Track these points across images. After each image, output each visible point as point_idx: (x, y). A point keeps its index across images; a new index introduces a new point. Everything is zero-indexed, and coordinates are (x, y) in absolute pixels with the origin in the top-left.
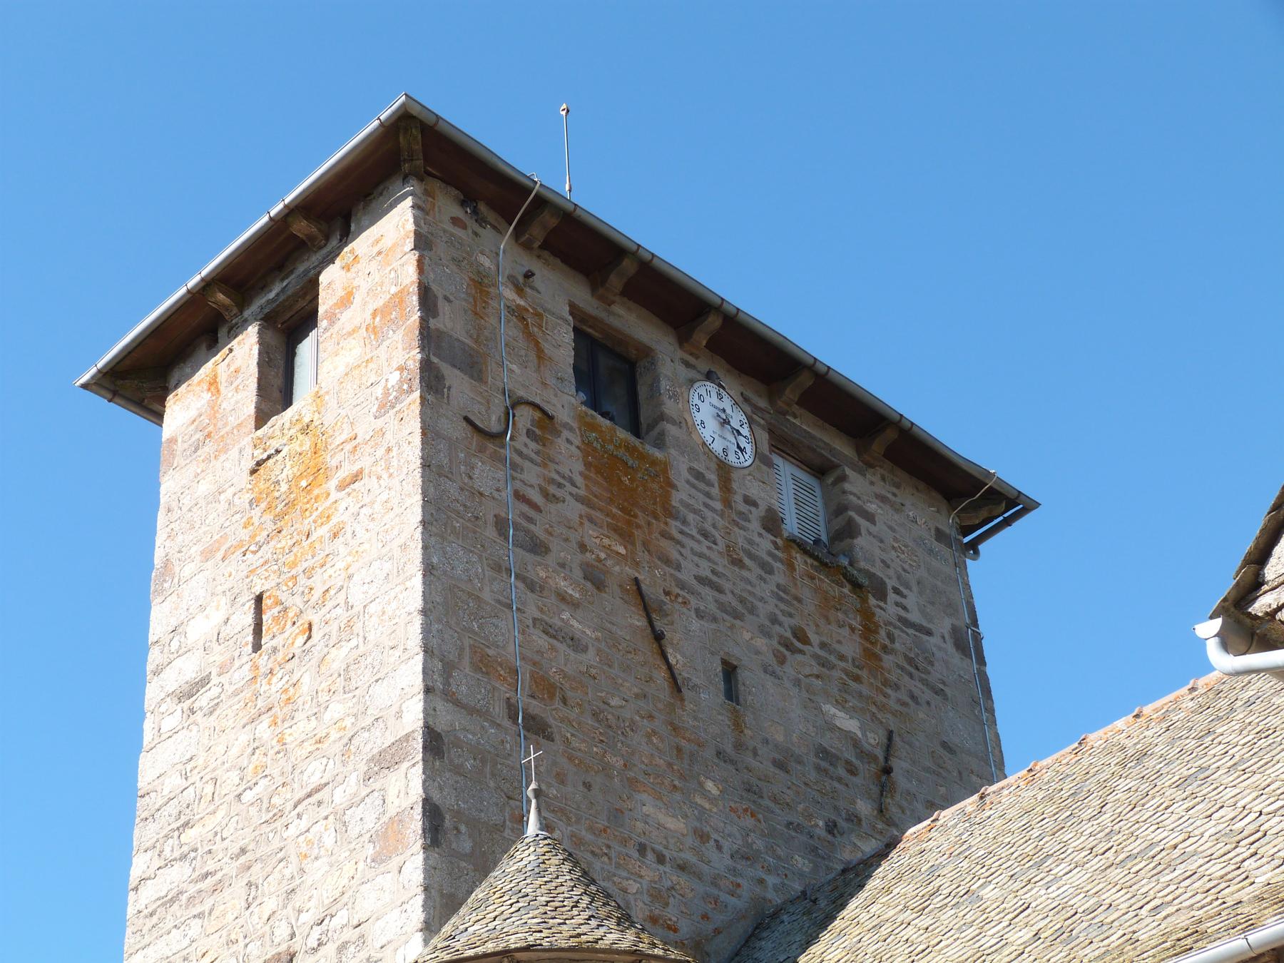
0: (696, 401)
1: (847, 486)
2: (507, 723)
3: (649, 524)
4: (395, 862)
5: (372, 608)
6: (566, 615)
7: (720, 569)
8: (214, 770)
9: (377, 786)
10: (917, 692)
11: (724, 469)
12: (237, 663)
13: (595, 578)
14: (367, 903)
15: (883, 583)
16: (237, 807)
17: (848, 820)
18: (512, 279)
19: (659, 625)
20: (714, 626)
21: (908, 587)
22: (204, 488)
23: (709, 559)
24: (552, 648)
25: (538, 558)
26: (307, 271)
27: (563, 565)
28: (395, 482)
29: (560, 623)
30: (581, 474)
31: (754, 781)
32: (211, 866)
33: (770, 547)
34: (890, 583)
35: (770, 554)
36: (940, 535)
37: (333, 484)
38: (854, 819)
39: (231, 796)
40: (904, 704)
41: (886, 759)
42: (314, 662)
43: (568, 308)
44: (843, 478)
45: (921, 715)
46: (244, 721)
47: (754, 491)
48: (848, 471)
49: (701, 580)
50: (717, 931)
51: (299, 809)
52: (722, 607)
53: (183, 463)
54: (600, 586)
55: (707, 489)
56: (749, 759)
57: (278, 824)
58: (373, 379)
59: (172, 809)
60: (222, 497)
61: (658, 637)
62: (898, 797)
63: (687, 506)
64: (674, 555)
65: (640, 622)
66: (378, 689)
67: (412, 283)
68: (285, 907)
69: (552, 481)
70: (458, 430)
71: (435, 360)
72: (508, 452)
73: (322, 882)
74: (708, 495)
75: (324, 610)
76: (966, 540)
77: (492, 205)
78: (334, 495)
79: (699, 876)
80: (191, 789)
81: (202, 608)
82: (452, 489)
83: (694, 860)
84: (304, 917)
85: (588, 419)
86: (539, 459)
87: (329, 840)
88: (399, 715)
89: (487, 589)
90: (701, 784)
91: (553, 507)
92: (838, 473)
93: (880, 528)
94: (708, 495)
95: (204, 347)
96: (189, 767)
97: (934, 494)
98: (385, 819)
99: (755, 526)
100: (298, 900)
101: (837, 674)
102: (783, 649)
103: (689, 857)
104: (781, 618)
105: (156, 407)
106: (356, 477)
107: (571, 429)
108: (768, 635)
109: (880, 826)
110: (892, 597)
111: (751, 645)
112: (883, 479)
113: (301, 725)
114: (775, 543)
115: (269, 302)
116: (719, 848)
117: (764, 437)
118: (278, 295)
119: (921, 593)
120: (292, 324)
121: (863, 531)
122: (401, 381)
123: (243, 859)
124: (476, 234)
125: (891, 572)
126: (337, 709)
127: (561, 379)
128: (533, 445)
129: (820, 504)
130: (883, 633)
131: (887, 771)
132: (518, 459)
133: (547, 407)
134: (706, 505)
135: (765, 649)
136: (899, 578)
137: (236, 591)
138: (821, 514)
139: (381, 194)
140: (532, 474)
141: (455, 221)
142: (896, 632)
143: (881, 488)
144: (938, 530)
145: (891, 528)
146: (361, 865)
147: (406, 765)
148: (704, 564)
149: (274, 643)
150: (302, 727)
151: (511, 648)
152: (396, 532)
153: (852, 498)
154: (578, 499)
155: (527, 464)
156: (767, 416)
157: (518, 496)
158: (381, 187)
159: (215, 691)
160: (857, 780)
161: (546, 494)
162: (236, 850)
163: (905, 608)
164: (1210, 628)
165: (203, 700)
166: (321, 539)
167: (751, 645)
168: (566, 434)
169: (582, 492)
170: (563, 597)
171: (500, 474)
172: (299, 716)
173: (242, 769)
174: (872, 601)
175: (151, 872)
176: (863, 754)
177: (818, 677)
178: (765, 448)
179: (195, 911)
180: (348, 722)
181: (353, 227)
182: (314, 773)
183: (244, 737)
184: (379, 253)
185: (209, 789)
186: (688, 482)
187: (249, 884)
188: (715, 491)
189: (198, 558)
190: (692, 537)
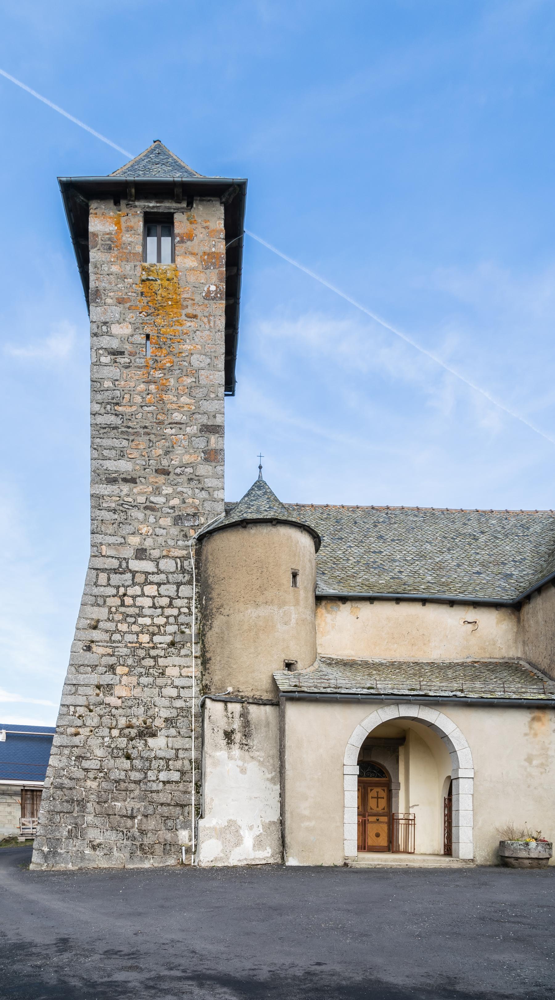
46: (144, 380)
118: (154, 207)
139: (209, 201)
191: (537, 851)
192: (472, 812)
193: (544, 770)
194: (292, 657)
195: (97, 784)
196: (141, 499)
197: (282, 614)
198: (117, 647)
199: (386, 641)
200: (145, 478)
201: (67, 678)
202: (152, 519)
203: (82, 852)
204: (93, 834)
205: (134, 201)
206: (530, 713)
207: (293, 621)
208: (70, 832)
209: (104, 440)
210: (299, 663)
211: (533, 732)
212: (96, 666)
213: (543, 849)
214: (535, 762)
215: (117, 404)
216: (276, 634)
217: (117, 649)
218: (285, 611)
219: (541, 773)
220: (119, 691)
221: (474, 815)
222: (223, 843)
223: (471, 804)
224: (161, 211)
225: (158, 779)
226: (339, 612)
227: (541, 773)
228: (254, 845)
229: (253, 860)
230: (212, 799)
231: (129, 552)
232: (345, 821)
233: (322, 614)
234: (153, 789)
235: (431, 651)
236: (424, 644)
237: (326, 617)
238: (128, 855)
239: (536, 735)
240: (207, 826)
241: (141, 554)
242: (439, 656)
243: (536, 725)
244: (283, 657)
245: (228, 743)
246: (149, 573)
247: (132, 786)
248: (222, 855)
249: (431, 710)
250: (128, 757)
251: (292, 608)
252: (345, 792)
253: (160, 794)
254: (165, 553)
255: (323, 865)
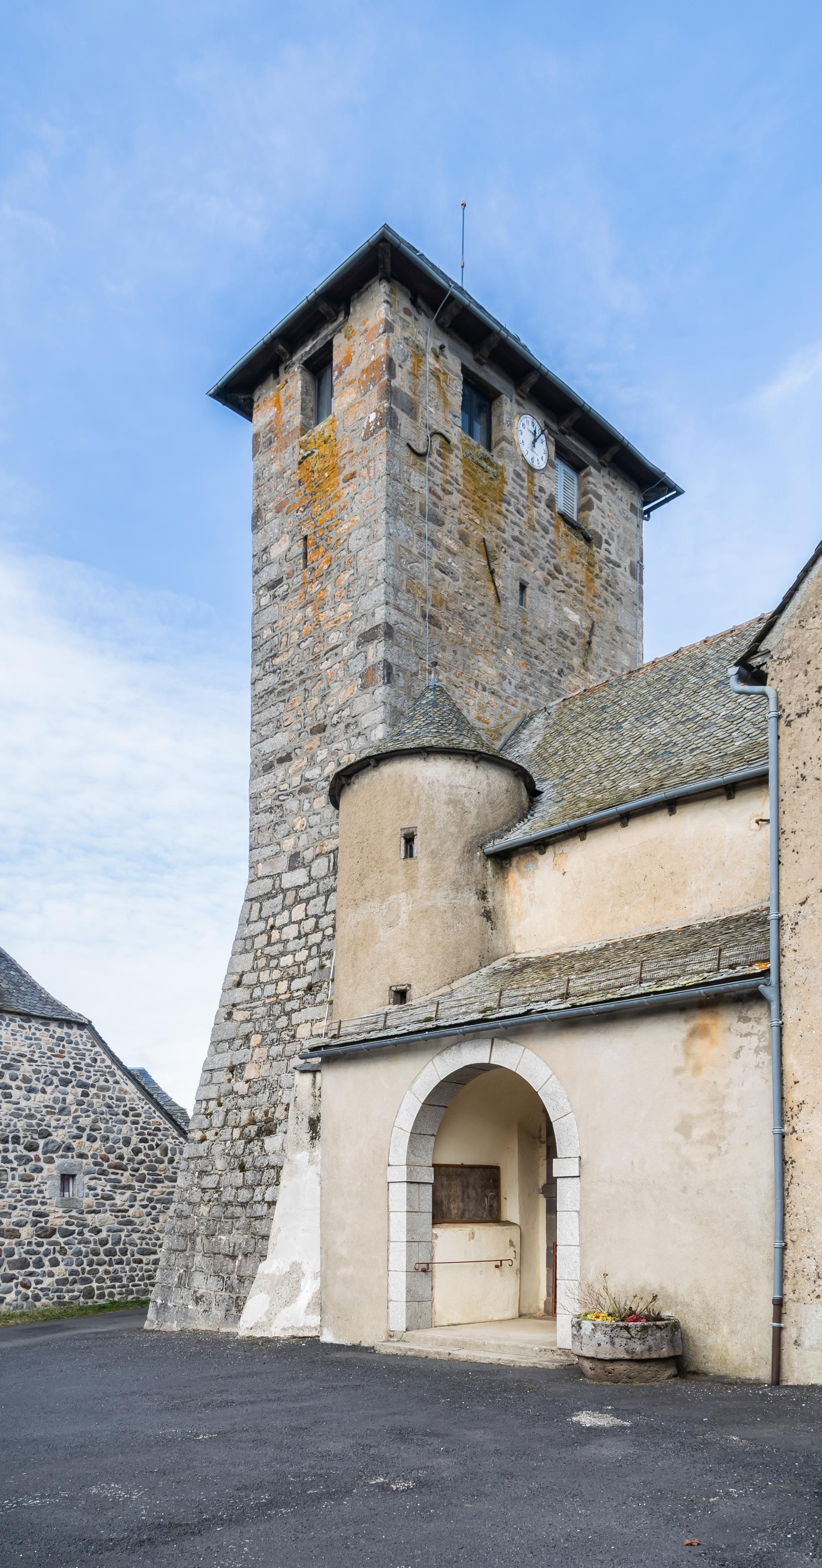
0: (521, 428)
1: (590, 479)
2: (421, 620)
3: (492, 506)
4: (371, 689)
5: (361, 554)
6: (450, 560)
7: (524, 531)
8: (287, 629)
9: (363, 650)
10: (608, 599)
11: (531, 470)
12: (296, 574)
13: (464, 538)
14: (358, 708)
15: (601, 537)
16: (298, 650)
17: (568, 668)
18: (434, 351)
19: (493, 566)
20: (518, 565)
21: (613, 540)
22: (275, 467)
23: (519, 526)
24: (443, 580)
25: (439, 528)
26: (326, 337)
27: (450, 532)
28: (373, 482)
29: (447, 565)
30: (462, 476)
31: (529, 649)
32: (287, 678)
33: (548, 517)
34: (604, 537)
35: (548, 522)
36: (633, 508)
37: (341, 477)
38: (571, 668)
39: (295, 645)
40: (602, 607)
41: (590, 636)
42: (332, 579)
43: (460, 368)
44: (589, 474)
45: (609, 612)
46: (300, 606)
47: (545, 483)
48: (592, 469)
49: (515, 539)
50: (506, 724)
51: (327, 656)
52: (522, 553)
53: (264, 451)
54: (467, 544)
55: (521, 483)
56: (528, 638)
57: (317, 662)
58: (362, 415)
59: (267, 646)
60: (285, 475)
61: (492, 572)
62: (592, 656)
63: (511, 494)
64: (503, 524)
65: (484, 563)
66: (363, 599)
67: (383, 356)
68: (321, 703)
69: (448, 482)
70: (405, 453)
71: (393, 407)
72: (427, 465)
73: (339, 695)
74: (522, 487)
75: (337, 551)
76: (645, 508)
77: (426, 300)
78: (342, 485)
79: (500, 697)
80: (276, 638)
81: (277, 540)
82: (400, 487)
83: (498, 689)
84: (330, 709)
85: (466, 442)
86: (441, 468)
87: (341, 673)
88: (373, 614)
89: (415, 546)
90: (505, 650)
91: (446, 497)
92: (587, 470)
93: (603, 505)
94: (522, 487)
95: (272, 376)
96: (275, 626)
97: (633, 483)
98: (367, 667)
99: (543, 505)
100: (328, 701)
101: (572, 590)
102: (549, 577)
103: (496, 687)
104: (550, 559)
105: (248, 409)
106: (353, 475)
107: (458, 449)
108: (543, 569)
109: (582, 671)
110: (604, 546)
111: (535, 574)
112: (609, 474)
113: (327, 612)
114: (551, 515)
115: (306, 353)
116: (510, 683)
117: (553, 449)
118: (311, 349)
119: (618, 543)
120: (319, 368)
121: (595, 507)
122: (376, 420)
123: (302, 677)
124: (416, 319)
125: (606, 531)
126: (343, 607)
127: (455, 416)
128: (440, 460)
129: (576, 488)
130: (597, 567)
131: (589, 643)
132: (432, 469)
133: (447, 435)
134: (520, 493)
135: (540, 577)
136: (609, 534)
137: (293, 533)
138: (576, 494)
139: (367, 289)
140: (438, 477)
141: (407, 312)
142: (604, 566)
143: (608, 480)
144: (632, 505)
145: (609, 504)
146: (356, 689)
147: (376, 641)
148: (517, 529)
149: (313, 565)
150: (328, 613)
151: (424, 580)
152: (372, 513)
153: (592, 486)
154: (458, 491)
155: (436, 472)
156: (555, 435)
157: (431, 491)
158: (367, 285)
159: (286, 587)
160: (575, 648)
161: (444, 490)
162: (298, 671)
163: (609, 552)
164: (733, 670)
165: (280, 590)
166: (335, 509)
167: (535, 574)
168: (456, 451)
169: (461, 488)
170: (449, 550)
171: (423, 479)
172: (326, 607)
173: (300, 631)
174: (595, 548)
175: (260, 677)
176: (579, 634)
177: (563, 592)
178: (553, 455)
179: (282, 698)
180: (350, 614)
181: (351, 310)
182: (334, 638)
183: (300, 615)
184: (366, 331)
185: (284, 639)
186: (513, 479)
187: (305, 690)
188: (525, 484)
189: (274, 510)
190: (512, 513)
191: (594, 1342)
192: (577, 1250)
193: (716, 1149)
194: (400, 980)
195: (208, 1209)
196: (296, 781)
197: (385, 911)
198: (256, 1007)
199: (611, 904)
200: (300, 748)
201: (205, 1064)
202: (306, 806)
203: (185, 1306)
204: (198, 1281)
205: (291, 358)
206: (686, 1021)
207: (404, 917)
208: (180, 1278)
209: (262, 715)
210: (414, 987)
211: (692, 1063)
212: (234, 1039)
213: (607, 1339)
214: (697, 1133)
215: (275, 656)
216: (377, 946)
217: (255, 1010)
218: (390, 904)
219: (711, 1157)
220: (250, 1072)
221: (583, 1255)
222: (273, 1299)
223: (577, 1232)
224: (318, 348)
225: (263, 1200)
226: (537, 872)
227: (711, 1157)
228: (309, 1304)
229: (301, 1329)
230: (279, 1230)
231: (283, 863)
232: (391, 1267)
233: (515, 882)
234: (258, 1214)
235: (691, 903)
236: (676, 892)
237: (520, 885)
238: (223, 1312)
239: (697, 1069)
240: (266, 1272)
241: (295, 862)
242: (708, 909)
243: (700, 1046)
244: (389, 982)
245: (312, 1138)
246: (300, 887)
247: (238, 1211)
248: (265, 1319)
249: (511, 1045)
250: (242, 1168)
251: (403, 895)
252: (392, 1215)
253: (264, 1221)
254: (318, 851)
255: (362, 1345)
